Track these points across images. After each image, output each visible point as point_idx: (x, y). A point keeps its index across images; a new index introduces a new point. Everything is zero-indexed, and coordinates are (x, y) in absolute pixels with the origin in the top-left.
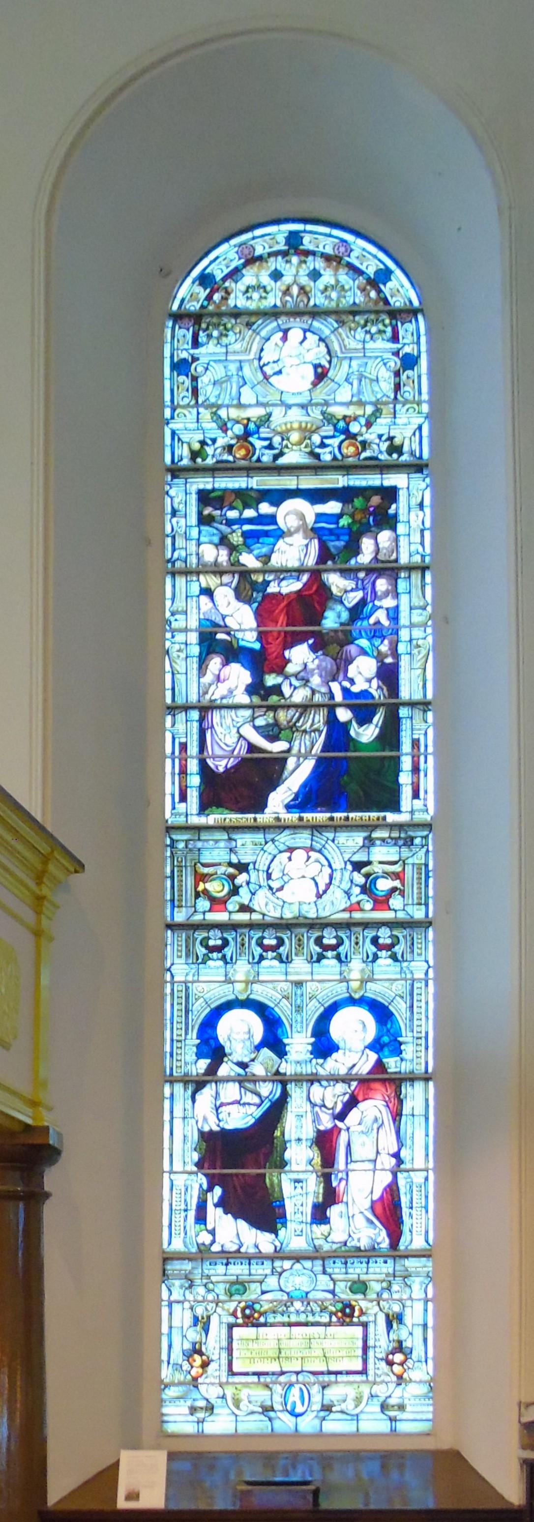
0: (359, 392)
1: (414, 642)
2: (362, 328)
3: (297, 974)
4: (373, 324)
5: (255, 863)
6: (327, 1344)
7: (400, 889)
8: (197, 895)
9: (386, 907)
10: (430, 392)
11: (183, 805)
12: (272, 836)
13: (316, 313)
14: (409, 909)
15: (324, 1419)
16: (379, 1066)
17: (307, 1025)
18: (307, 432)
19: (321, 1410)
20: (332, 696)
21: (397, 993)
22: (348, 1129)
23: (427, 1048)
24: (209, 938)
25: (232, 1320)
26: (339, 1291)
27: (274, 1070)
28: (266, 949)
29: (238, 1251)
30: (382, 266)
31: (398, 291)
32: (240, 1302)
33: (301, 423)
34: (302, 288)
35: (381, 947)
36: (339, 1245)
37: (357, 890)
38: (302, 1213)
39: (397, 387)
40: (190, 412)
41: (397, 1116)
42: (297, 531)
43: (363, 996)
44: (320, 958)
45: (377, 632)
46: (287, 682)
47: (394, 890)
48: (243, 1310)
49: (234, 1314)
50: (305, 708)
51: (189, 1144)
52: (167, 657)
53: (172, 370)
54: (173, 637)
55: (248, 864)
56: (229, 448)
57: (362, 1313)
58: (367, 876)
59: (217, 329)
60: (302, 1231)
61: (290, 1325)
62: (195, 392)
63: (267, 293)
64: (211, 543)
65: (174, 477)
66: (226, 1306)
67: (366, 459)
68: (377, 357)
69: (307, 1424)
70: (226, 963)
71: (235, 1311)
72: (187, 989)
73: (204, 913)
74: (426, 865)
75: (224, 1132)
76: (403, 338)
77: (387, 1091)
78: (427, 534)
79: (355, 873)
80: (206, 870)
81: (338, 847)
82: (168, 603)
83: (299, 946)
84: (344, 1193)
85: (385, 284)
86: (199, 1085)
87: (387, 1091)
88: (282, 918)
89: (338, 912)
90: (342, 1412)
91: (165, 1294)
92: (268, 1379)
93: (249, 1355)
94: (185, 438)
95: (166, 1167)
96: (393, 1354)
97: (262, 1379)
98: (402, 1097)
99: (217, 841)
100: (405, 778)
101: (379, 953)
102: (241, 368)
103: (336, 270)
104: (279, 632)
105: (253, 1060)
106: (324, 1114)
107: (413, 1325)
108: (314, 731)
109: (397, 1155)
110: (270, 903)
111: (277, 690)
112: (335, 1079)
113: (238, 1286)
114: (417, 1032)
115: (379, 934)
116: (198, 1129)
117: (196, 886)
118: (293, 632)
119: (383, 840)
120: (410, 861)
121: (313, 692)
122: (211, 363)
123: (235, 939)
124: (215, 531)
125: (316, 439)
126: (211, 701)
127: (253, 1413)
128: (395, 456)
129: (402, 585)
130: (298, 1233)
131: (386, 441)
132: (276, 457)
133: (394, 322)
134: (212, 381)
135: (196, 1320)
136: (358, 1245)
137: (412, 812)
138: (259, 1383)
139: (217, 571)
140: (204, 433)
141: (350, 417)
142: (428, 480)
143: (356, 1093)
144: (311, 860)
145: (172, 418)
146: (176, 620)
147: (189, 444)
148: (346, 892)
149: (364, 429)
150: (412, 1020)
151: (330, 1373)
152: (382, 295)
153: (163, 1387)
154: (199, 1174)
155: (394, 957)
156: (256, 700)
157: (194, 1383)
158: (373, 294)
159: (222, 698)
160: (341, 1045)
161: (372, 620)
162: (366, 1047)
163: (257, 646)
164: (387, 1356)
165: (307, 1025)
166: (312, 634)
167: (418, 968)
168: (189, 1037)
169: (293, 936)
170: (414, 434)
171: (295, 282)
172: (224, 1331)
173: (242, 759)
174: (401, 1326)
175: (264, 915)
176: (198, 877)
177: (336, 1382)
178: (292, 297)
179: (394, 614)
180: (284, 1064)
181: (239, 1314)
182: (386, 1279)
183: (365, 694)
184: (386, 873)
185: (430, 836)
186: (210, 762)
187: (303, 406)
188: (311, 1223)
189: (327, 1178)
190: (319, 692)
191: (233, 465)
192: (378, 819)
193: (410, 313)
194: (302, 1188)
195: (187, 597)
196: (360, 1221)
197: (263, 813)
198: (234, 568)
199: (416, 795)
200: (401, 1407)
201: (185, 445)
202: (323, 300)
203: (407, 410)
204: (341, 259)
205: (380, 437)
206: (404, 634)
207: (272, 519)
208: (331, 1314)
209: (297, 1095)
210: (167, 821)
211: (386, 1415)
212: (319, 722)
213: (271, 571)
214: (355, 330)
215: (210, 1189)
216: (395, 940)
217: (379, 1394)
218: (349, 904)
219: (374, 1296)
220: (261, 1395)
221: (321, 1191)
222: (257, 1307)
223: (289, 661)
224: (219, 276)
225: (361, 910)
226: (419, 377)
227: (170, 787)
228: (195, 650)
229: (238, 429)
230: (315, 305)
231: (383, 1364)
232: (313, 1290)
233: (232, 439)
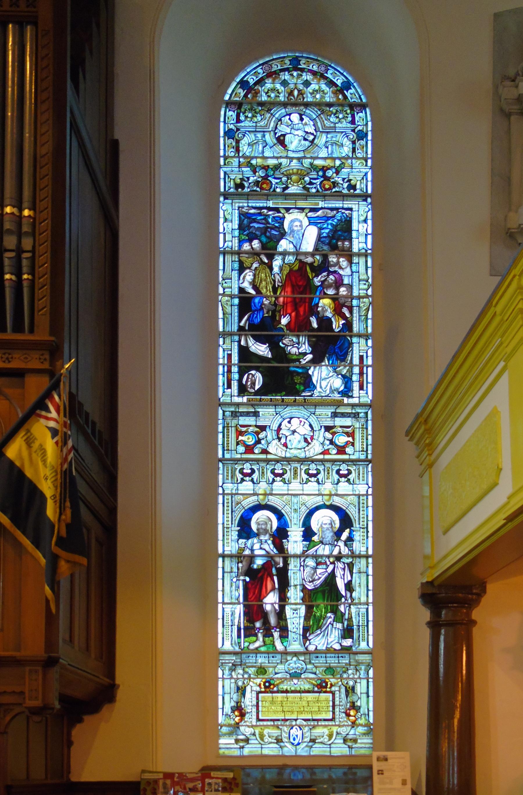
0: (332, 152)
2: (334, 115)
4: (340, 113)
8: (238, 444)
10: (372, 154)
11: (229, 390)
13: (307, 105)
15: (311, 747)
19: (309, 742)
24: (243, 469)
25: (258, 689)
28: (276, 475)
30: (345, 80)
34: (299, 91)
35: (341, 476)
47: (347, 443)
48: (265, 683)
56: (257, 183)
57: (332, 685)
59: (251, 113)
62: (238, 150)
63: (280, 94)
65: (225, 198)
66: (255, 681)
67: (336, 192)
68: (342, 132)
69: (302, 750)
73: (241, 454)
76: (358, 122)
79: (327, 433)
80: (244, 429)
82: (221, 273)
90: (321, 743)
91: (220, 675)
92: (279, 723)
94: (232, 177)
95: (220, 600)
97: (276, 723)
101: (275, 478)
102: (264, 136)
103: (319, 81)
110: (279, 448)
115: (341, 468)
117: (237, 438)
122: (247, 132)
125: (307, 179)
127: (271, 743)
128: (352, 191)
131: (347, 182)
132: (285, 189)
133: (352, 112)
134: (247, 143)
135: (238, 688)
138: (274, 726)
140: (243, 174)
141: (326, 167)
146: (226, 283)
149: (335, 175)
151: (314, 720)
153: (220, 727)
157: (237, 726)
158: (340, 97)
167: (362, 489)
170: (363, 179)
171: (296, 88)
172: (254, 695)
177: (318, 725)
178: (294, 97)
181: (262, 686)
191: (259, 193)
200: (355, 741)
201: (232, 181)
205: (343, 179)
214: (330, 116)
217: (342, 733)
219: (339, 676)
220: (275, 732)
222: (272, 682)
224: (252, 82)
227: (221, 380)
229: (262, 173)
231: (344, 715)
233: (259, 178)
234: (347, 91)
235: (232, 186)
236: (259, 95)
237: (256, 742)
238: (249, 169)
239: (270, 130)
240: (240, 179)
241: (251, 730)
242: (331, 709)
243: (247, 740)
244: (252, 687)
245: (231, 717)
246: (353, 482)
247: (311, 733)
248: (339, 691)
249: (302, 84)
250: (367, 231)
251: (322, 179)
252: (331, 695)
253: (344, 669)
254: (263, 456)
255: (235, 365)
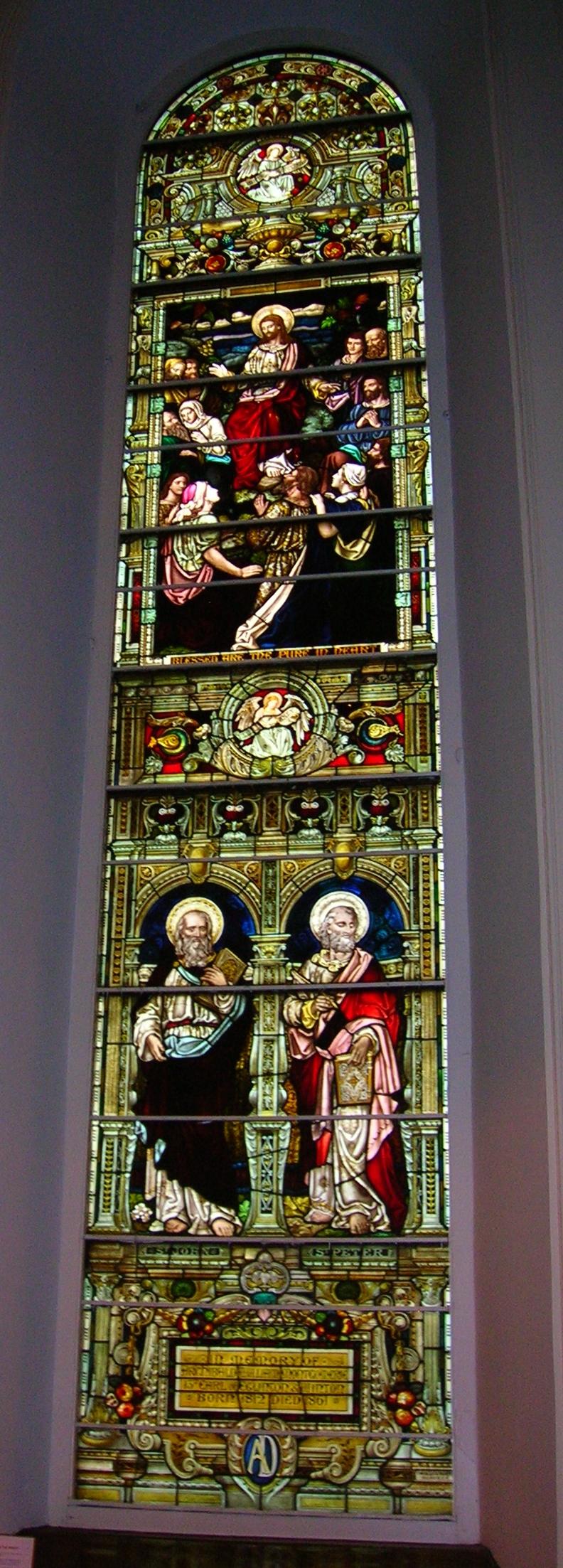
0: (343, 195)
1: (410, 444)
3: (269, 849)
5: (218, 711)
6: (304, 1374)
7: (398, 736)
8: (148, 752)
9: (379, 758)
11: (136, 645)
12: (238, 678)
14: (410, 761)
16: (375, 971)
17: (281, 917)
18: (284, 238)
19: (295, 1476)
20: (313, 508)
21: (396, 871)
22: (334, 1058)
23: (437, 944)
26: (322, 1295)
27: (237, 979)
29: (184, 1233)
31: (384, 100)
32: (186, 1309)
33: (279, 229)
35: (375, 812)
36: (321, 1227)
37: (344, 740)
38: (271, 1178)
39: (384, 188)
40: (161, 232)
41: (398, 1039)
42: (274, 336)
43: (353, 875)
44: (299, 826)
45: (366, 436)
46: (261, 498)
47: (391, 736)
49: (177, 1325)
50: (280, 527)
51: (126, 1081)
52: (124, 481)
53: (144, 195)
54: (132, 457)
55: (210, 712)
56: (201, 262)
58: (356, 721)
60: (271, 1206)
61: (254, 1343)
63: (246, 116)
64: (178, 357)
67: (351, 258)
70: (180, 837)
71: (180, 1320)
72: (131, 870)
73: (155, 775)
74: (432, 704)
75: (172, 1064)
77: (385, 1006)
78: (422, 328)
80: (160, 722)
81: (320, 687)
82: (129, 422)
83: (272, 812)
84: (328, 1152)
85: (369, 97)
86: (140, 1001)
87: (385, 1006)
88: (250, 778)
89: (320, 769)
90: (324, 1479)
93: (196, 1388)
96: (397, 1393)
98: (405, 1013)
99: (173, 686)
100: (402, 601)
102: (216, 186)
104: (251, 444)
105: (210, 965)
106: (302, 1039)
107: (425, 1348)
108: (292, 551)
109: (398, 1096)
111: (249, 507)
112: (314, 990)
113: (183, 1285)
114: (425, 923)
116: (138, 1058)
118: (268, 443)
119: (376, 675)
120: (411, 700)
121: (292, 506)
123: (192, 807)
124: (183, 345)
126: (171, 524)
127: (200, 1475)
129: (394, 384)
130: (266, 1207)
131: (373, 239)
135: (126, 1330)
136: (347, 1226)
137: (412, 641)
139: (184, 386)
142: (421, 274)
143: (343, 1008)
144: (288, 703)
145: (143, 238)
147: (159, 262)
148: (330, 742)
150: (416, 907)
152: (366, 105)
154: (138, 1124)
155: (391, 824)
156: (223, 520)
159: (184, 521)
160: (325, 942)
161: (360, 423)
162: (357, 945)
163: (227, 460)
164: (388, 1396)
165: (281, 917)
166: (292, 444)
168: (131, 934)
169: (265, 801)
170: (404, 230)
173: (207, 588)
174: (408, 1351)
175: (228, 774)
176: (150, 730)
179: (385, 416)
180: (250, 971)
181: (185, 1326)
182: (387, 1278)
183: (352, 504)
184: (382, 717)
185: (435, 669)
186: (168, 594)
187: (281, 215)
188: (284, 1195)
189: (302, 1130)
190: (298, 507)
192: (370, 650)
193: (396, 119)
194: (271, 1141)
195: (149, 414)
196: (349, 1192)
197: (230, 650)
198: (201, 380)
199: (416, 620)
200: (408, 1475)
201: (155, 265)
202: (304, 116)
203: (396, 208)
204: (324, 78)
205: (366, 236)
206: (398, 436)
207: (246, 326)
208: (311, 1328)
209: (266, 1022)
210: (115, 665)
211: (387, 1487)
212: (298, 540)
213: (243, 381)
215: (151, 1143)
216: (394, 802)
218: (334, 756)
221: (297, 1147)
222: (210, 1315)
223: (264, 474)
225: (351, 765)
226: (408, 176)
228: (157, 470)
230: (296, 120)
232: (285, 1293)
234: (369, 97)
235: (154, 272)
236: (210, 123)
237: (164, 1471)
238: (187, 241)
239: (229, 174)
240: (170, 259)
241: (150, 1440)
242: (350, 1388)
243: (141, 1466)
244: (159, 1326)
245: (109, 1403)
246: (403, 824)
247: (299, 1452)
248: (371, 1342)
249: (288, 96)
250: (417, 318)
251: (325, 240)
252: (350, 1353)
253: (384, 1286)
254: (204, 778)
255: (148, 589)
